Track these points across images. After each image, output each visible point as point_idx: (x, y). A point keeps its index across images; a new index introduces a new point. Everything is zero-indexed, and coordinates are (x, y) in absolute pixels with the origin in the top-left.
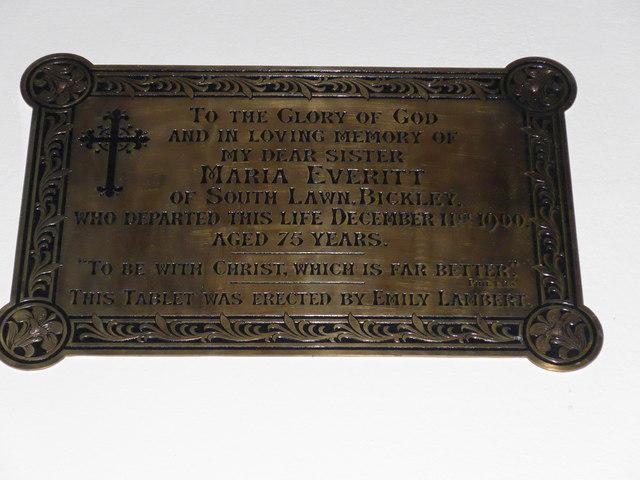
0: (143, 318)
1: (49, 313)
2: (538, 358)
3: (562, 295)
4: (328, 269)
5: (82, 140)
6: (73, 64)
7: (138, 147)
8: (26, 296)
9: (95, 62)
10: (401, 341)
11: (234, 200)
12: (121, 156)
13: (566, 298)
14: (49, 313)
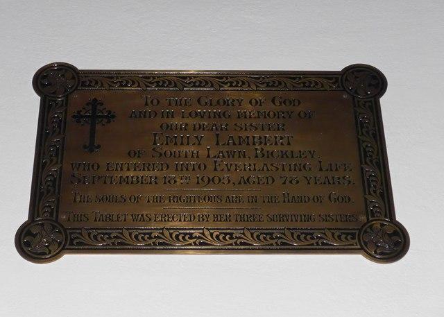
0: (274, 229)
1: (54, 227)
2: (372, 257)
3: (383, 213)
4: (200, 180)
5: (73, 117)
6: (64, 70)
7: (109, 122)
8: (38, 216)
9: (80, 68)
10: (277, 245)
11: (203, 178)
12: (98, 127)
13: (386, 216)
14: (54, 227)
